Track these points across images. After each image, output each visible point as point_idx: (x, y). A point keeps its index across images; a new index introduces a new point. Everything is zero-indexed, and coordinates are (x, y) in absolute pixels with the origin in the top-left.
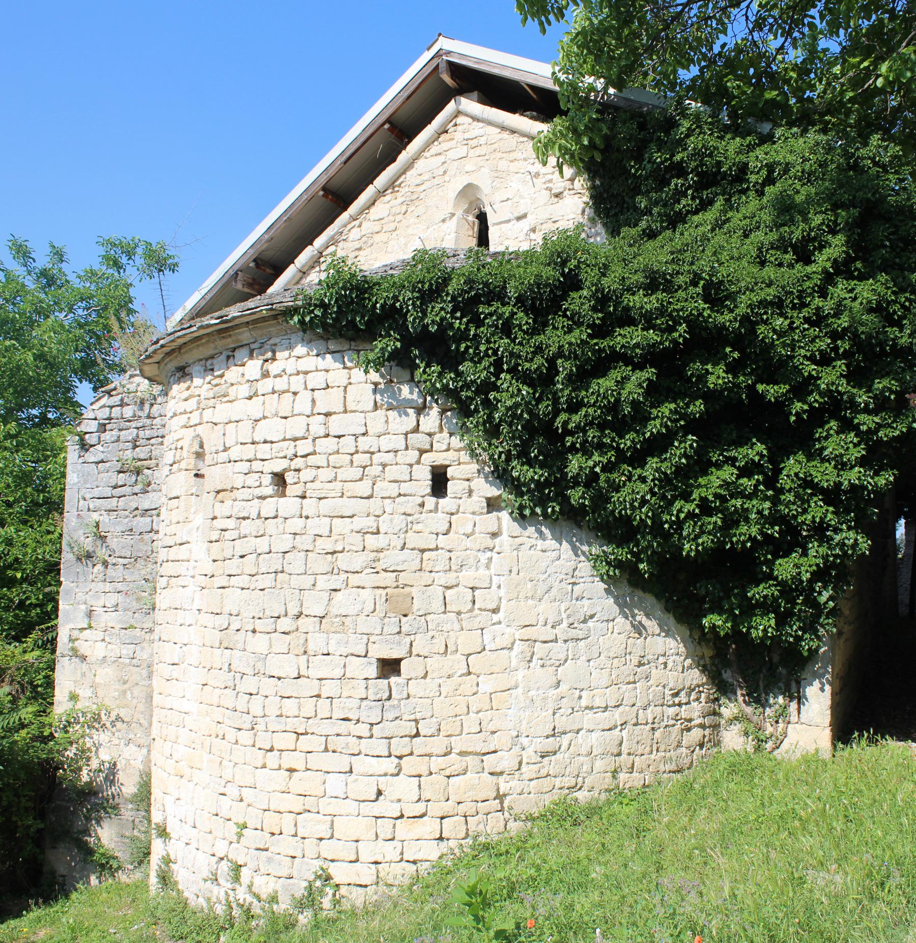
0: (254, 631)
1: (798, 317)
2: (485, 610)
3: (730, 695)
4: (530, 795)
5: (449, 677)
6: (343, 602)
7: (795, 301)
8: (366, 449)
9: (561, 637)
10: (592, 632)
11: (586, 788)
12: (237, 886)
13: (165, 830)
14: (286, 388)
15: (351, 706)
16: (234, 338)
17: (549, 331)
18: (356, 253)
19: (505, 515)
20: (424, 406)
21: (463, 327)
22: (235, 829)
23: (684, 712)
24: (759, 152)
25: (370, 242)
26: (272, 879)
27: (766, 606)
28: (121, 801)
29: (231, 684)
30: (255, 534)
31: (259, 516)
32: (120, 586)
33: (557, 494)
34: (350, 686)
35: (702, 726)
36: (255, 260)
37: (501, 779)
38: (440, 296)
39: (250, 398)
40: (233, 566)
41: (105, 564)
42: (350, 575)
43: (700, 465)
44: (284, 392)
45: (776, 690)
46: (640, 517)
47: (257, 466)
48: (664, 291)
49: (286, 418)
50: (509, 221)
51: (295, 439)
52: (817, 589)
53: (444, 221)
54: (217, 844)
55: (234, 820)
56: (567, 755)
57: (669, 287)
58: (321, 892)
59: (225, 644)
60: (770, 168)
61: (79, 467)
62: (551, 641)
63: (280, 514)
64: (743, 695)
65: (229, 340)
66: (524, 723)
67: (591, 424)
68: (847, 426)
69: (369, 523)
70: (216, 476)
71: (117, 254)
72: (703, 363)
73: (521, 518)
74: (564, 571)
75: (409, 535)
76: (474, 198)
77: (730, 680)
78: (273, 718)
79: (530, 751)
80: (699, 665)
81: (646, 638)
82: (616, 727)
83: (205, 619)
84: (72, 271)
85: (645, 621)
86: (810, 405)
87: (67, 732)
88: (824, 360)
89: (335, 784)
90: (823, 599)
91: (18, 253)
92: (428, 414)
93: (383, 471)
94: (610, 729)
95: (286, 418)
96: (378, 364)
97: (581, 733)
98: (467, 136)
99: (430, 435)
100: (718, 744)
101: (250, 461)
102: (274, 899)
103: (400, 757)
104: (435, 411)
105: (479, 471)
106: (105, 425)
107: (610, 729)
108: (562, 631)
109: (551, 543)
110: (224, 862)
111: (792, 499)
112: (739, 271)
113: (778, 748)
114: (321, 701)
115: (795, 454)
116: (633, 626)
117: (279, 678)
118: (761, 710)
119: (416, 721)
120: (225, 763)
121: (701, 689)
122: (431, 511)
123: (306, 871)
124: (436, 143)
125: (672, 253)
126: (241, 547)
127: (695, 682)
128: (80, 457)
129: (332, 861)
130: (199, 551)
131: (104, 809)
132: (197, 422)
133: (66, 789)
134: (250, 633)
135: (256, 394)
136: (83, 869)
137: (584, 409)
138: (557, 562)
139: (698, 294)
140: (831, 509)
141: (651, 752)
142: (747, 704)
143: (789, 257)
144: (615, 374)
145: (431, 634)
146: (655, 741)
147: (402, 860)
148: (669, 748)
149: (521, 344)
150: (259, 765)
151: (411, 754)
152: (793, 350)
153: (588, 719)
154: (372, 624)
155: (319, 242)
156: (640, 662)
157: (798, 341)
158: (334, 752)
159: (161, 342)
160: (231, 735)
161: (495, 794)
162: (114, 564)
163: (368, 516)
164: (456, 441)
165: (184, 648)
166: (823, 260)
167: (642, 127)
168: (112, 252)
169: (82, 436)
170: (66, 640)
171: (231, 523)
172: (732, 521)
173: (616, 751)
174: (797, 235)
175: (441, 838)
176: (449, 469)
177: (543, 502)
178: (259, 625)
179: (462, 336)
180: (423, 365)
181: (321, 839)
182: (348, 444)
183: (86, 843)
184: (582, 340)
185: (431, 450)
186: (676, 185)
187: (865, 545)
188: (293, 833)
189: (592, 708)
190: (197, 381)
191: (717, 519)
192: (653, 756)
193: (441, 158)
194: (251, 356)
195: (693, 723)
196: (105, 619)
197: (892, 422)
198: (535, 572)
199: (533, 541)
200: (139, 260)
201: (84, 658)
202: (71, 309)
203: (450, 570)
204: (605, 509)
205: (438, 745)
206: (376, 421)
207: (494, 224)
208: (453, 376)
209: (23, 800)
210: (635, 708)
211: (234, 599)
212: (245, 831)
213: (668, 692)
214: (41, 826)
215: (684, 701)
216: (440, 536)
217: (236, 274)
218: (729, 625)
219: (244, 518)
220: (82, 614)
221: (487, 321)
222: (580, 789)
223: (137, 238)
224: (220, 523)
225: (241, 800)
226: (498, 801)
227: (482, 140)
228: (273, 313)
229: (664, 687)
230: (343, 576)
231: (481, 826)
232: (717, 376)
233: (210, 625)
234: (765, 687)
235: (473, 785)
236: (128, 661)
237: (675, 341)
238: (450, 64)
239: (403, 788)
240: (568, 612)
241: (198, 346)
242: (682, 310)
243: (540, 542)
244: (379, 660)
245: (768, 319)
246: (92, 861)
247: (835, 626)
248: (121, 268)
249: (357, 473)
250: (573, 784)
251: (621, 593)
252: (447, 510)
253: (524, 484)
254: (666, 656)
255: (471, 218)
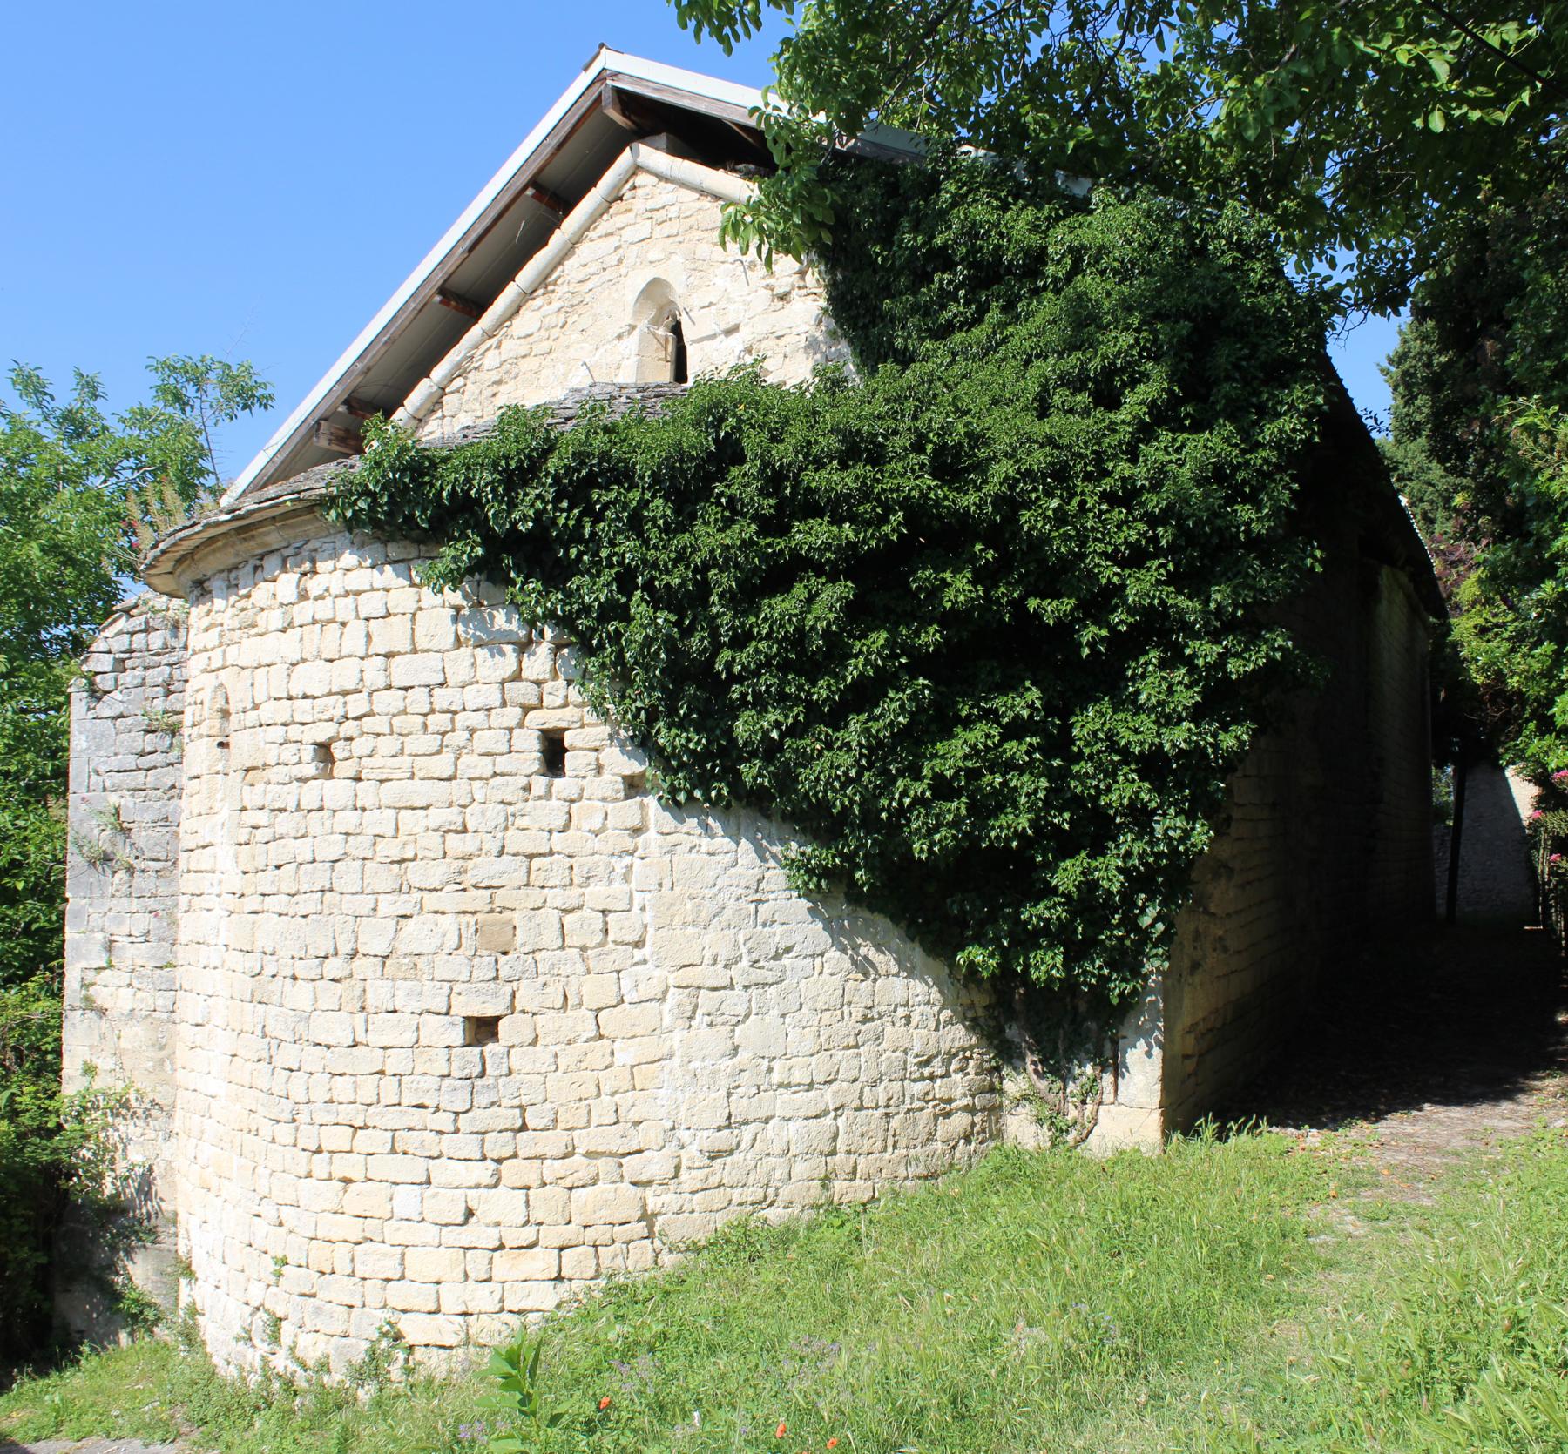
0: (294, 978)
1: (1090, 493)
2: (622, 943)
3: (1017, 1063)
4: (693, 1215)
5: (569, 1043)
6: (416, 934)
7: (1089, 468)
8: (445, 707)
9: (739, 981)
10: (789, 973)
11: (780, 1202)
12: (277, 1349)
13: (189, 1267)
14: (330, 616)
15: (426, 1086)
16: (259, 540)
17: (698, 527)
18: (494, 389)
19: (651, 801)
20: (530, 642)
21: (571, 523)
22: (272, 1267)
23: (939, 1089)
24: (1060, 231)
25: (515, 371)
26: (322, 1338)
27: (1058, 935)
28: (160, 1222)
29: (265, 1055)
30: (293, 834)
31: (298, 809)
32: (152, 903)
33: (724, 770)
34: (425, 1057)
35: (970, 1110)
36: (346, 402)
37: (650, 1191)
38: (536, 476)
39: (284, 631)
40: (266, 881)
41: (130, 870)
42: (425, 894)
43: (935, 722)
44: (328, 622)
45: (1083, 1055)
46: (842, 804)
47: (295, 732)
48: (867, 462)
49: (331, 661)
50: (713, 337)
51: (345, 693)
52: (1140, 903)
53: (620, 337)
54: (251, 1287)
55: (272, 1253)
56: (749, 1156)
57: (877, 457)
58: (388, 1356)
59: (257, 998)
60: (1076, 253)
61: (89, 724)
62: (724, 988)
63: (326, 805)
64: (1034, 1063)
65: (252, 543)
66: (683, 1108)
67: (768, 664)
68: (1174, 658)
69: (452, 817)
70: (245, 747)
71: (180, 384)
72: (937, 570)
73: (675, 806)
74: (743, 884)
75: (509, 833)
76: (664, 301)
77: (1017, 1040)
78: (320, 1105)
79: (693, 1150)
80: (965, 1018)
81: (875, 980)
82: (826, 1113)
83: (235, 959)
84: (112, 410)
85: (874, 955)
86: (1112, 629)
87: (82, 1122)
88: (1135, 558)
89: (407, 1201)
90: (1145, 921)
91: (26, 387)
92: (534, 654)
93: (470, 740)
94: (816, 1117)
95: (331, 661)
96: (454, 579)
97: (772, 1122)
98: (651, 204)
99: (538, 683)
100: (999, 1134)
101: (285, 725)
102: (324, 1367)
103: (499, 1161)
104: (543, 650)
105: (611, 737)
106: (123, 660)
107: (816, 1117)
108: (738, 972)
109: (723, 842)
110: (261, 1313)
111: (1091, 771)
112: (1005, 427)
113: (1083, 1141)
114: (386, 1079)
115: (1098, 700)
116: (854, 963)
117: (328, 1047)
118: (1059, 1084)
119: (522, 1108)
120: (260, 1170)
121: (968, 1054)
122: (540, 798)
123: (367, 1326)
124: (605, 217)
125: (887, 401)
126: (277, 853)
127: (957, 1044)
128: (89, 709)
129: (404, 1311)
130: (224, 857)
131: (136, 1233)
132: (219, 665)
133: (83, 1205)
134: (288, 980)
135: (290, 625)
136: (109, 1322)
137: (754, 643)
138: (733, 870)
139: (922, 466)
140: (1146, 785)
141: (885, 1150)
142: (1040, 1076)
143: (1083, 398)
144: (800, 591)
145: (542, 979)
146: (891, 1132)
147: (502, 1310)
148: (912, 1143)
149: (656, 547)
150: (303, 1174)
151: (515, 1156)
152: (1083, 544)
153: (783, 1102)
154: (455, 967)
155: (439, 372)
156: (865, 1016)
157: (1093, 529)
158: (405, 1153)
159: (162, 546)
160: (267, 1129)
161: (639, 1214)
162: (143, 871)
163: (450, 806)
164: (574, 693)
165: (210, 1001)
166: (1135, 403)
167: (892, 190)
168: (172, 381)
169: (90, 679)
170: (77, 986)
171: (262, 818)
172: (987, 807)
173: (826, 1150)
174: (1094, 366)
175: (559, 1278)
176: (567, 734)
177: (704, 781)
178: (301, 969)
179: (574, 536)
180: (519, 580)
181: (388, 1280)
182: (419, 700)
183: (112, 1284)
184: (743, 541)
185: (540, 706)
186: (941, 281)
187: (1204, 838)
188: (349, 1271)
189: (789, 1086)
190: (219, 603)
191: (959, 806)
192: (887, 1156)
193: (614, 241)
194: (284, 569)
195: (954, 1105)
196: (131, 953)
197: (1244, 651)
198: (698, 886)
199: (696, 840)
200: (214, 394)
201: (102, 1012)
202: (112, 473)
203: (571, 884)
204: (796, 791)
205: (553, 1142)
206: (459, 663)
207: (694, 342)
208: (560, 596)
209: (16, 1222)
210: (858, 1085)
211: (269, 931)
212: (285, 1270)
213: (911, 1060)
214: (43, 1260)
215: (939, 1072)
216: (555, 835)
217: (318, 423)
218: (992, 962)
219: (280, 810)
220: (99, 947)
221: (608, 513)
222: (771, 1204)
223: (208, 357)
224: (251, 817)
225: (281, 1224)
226: (644, 1223)
227: (673, 211)
228: (299, 506)
229: (905, 1052)
230: (416, 895)
231: (619, 1260)
232: (959, 588)
233: (239, 968)
234: (1065, 1051)
235: (609, 1200)
236: (165, 1016)
237: (886, 537)
238: (620, 93)
239: (503, 1206)
240: (749, 944)
241: (214, 551)
242: (897, 490)
243: (705, 841)
244: (467, 1019)
245: (1038, 498)
246: (123, 1314)
247: (1168, 958)
248: (186, 404)
249: (432, 742)
250: (760, 1196)
251: (835, 913)
252: (564, 795)
253: (674, 755)
254: (907, 1007)
255: (662, 332)
